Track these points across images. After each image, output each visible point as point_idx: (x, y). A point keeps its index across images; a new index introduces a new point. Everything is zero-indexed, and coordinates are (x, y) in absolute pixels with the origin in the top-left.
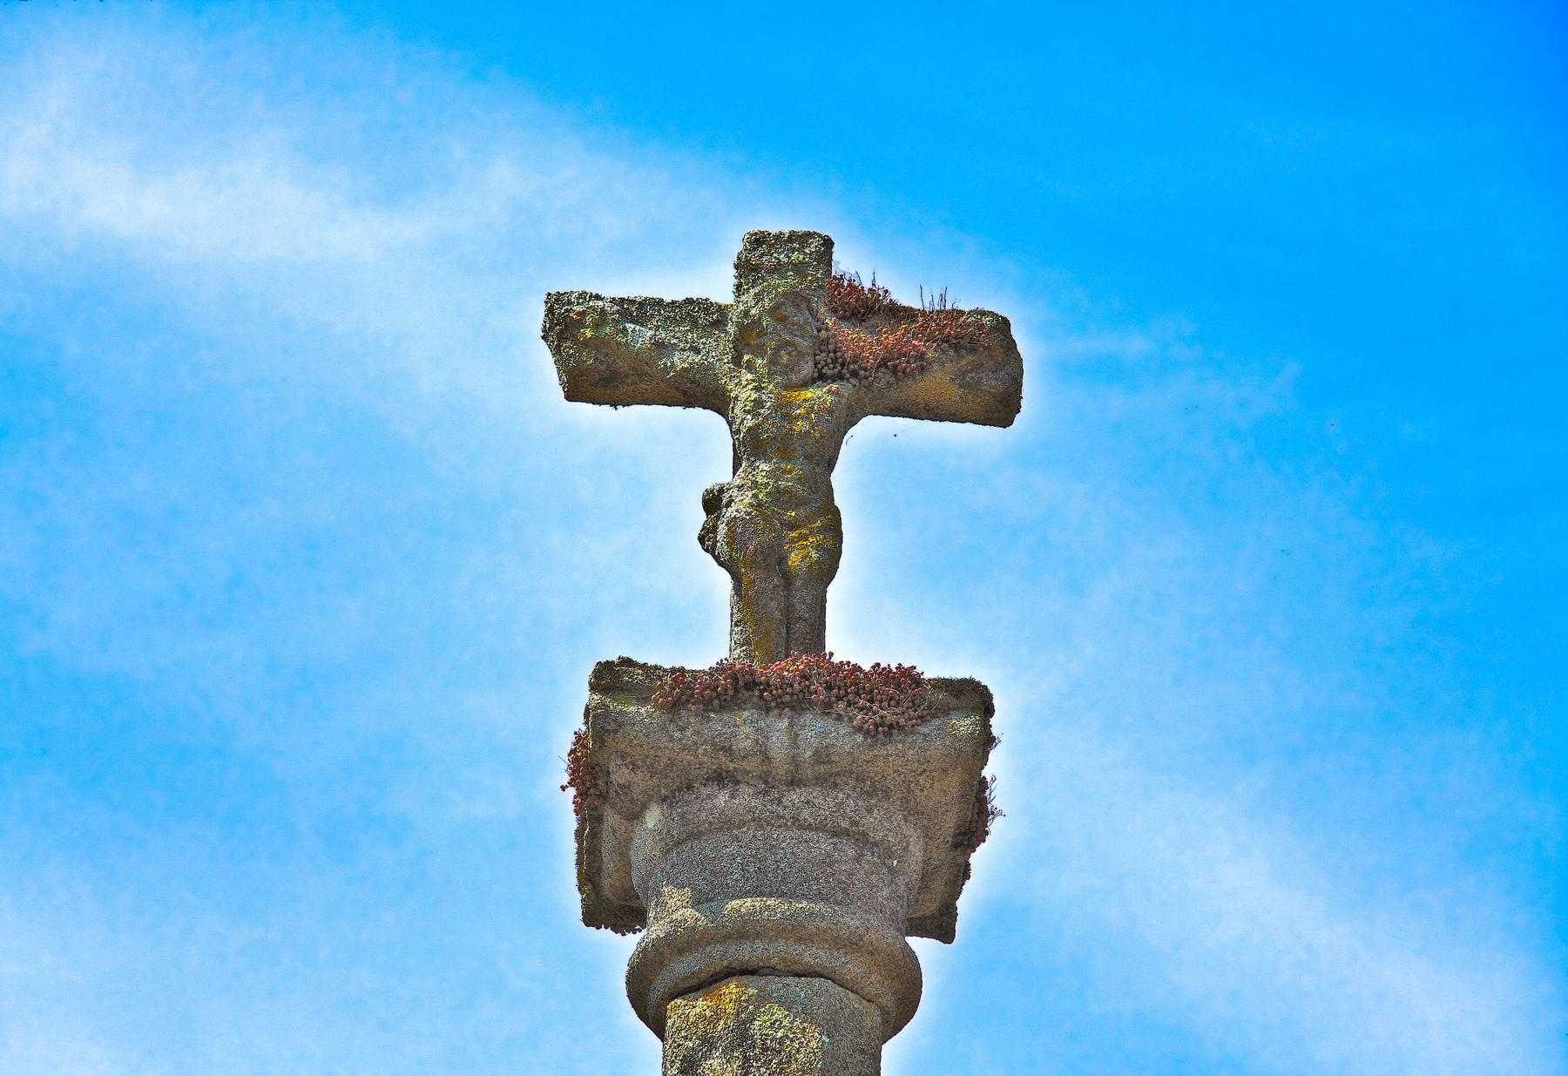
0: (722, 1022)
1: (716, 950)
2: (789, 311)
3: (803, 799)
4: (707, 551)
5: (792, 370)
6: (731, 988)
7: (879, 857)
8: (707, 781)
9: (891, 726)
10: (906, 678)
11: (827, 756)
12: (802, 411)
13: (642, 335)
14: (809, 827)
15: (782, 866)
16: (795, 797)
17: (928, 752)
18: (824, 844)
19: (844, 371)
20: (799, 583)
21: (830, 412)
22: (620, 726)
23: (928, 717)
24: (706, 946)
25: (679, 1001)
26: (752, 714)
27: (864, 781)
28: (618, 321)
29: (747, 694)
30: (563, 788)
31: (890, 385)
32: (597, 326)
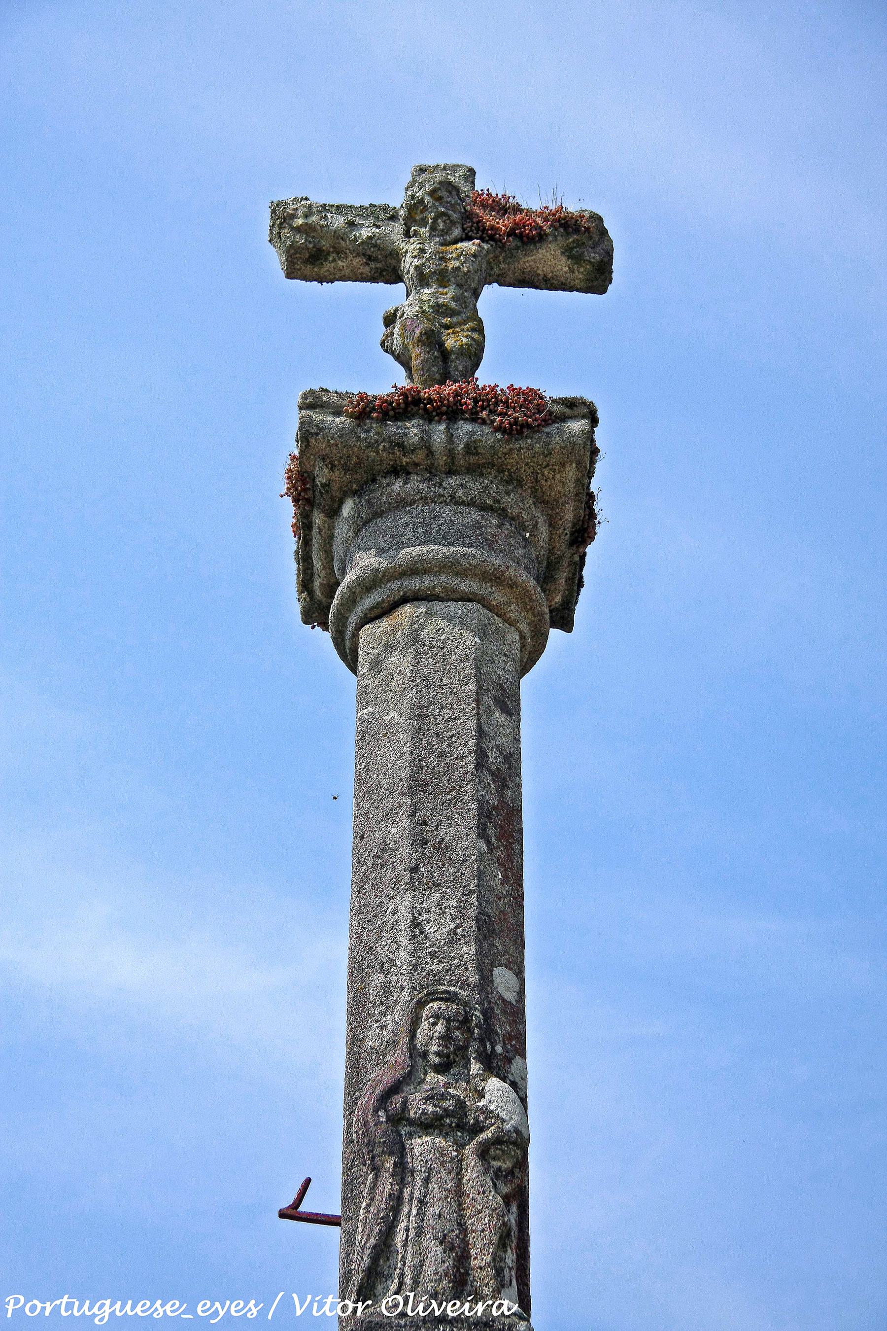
0: (399, 633)
1: (395, 585)
2: (443, 193)
3: (458, 483)
4: (386, 351)
5: (447, 233)
6: (407, 610)
7: (516, 528)
8: (387, 474)
9: (522, 426)
11: (475, 448)
12: (454, 255)
13: (338, 222)
14: (463, 503)
15: (443, 528)
17: (550, 446)
18: (476, 516)
19: (485, 235)
20: (453, 357)
21: (474, 256)
22: (320, 430)
23: (550, 422)
24: (387, 583)
25: (368, 626)
26: (418, 421)
27: (503, 471)
28: (321, 212)
29: (415, 409)
30: (282, 496)
31: (517, 248)
32: (306, 216)
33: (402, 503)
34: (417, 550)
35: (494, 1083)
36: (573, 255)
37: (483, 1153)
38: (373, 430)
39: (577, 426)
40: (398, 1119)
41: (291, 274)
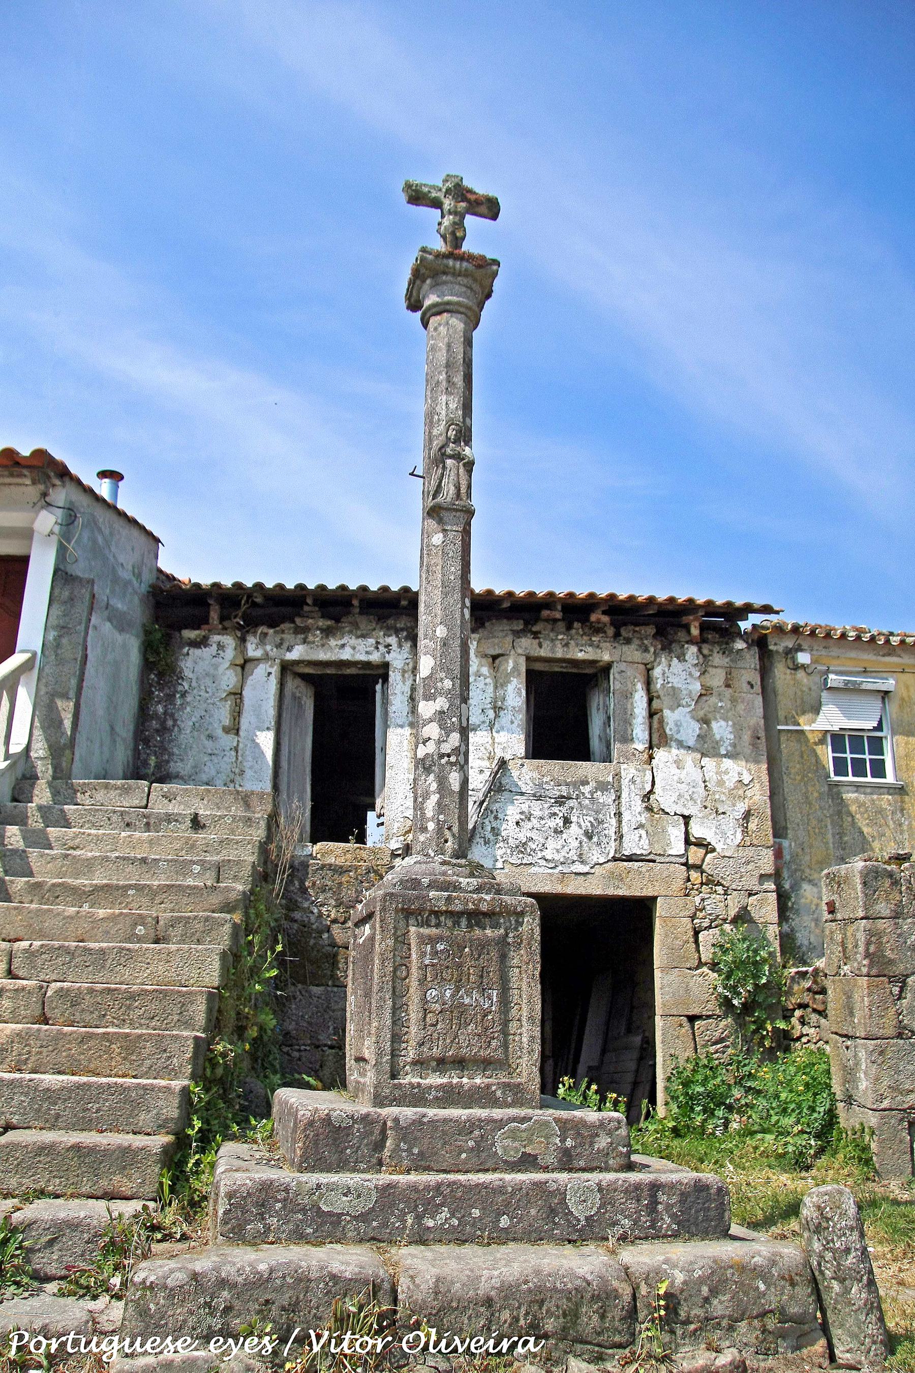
1: (442, 307)
6: (445, 314)
10: (483, 258)
13: (426, 190)
16: (459, 278)
33: (445, 283)
34: (450, 298)
35: (467, 448)
36: (489, 208)
37: (464, 465)
38: (439, 261)
39: (495, 267)
40: (443, 454)
41: (408, 202)
